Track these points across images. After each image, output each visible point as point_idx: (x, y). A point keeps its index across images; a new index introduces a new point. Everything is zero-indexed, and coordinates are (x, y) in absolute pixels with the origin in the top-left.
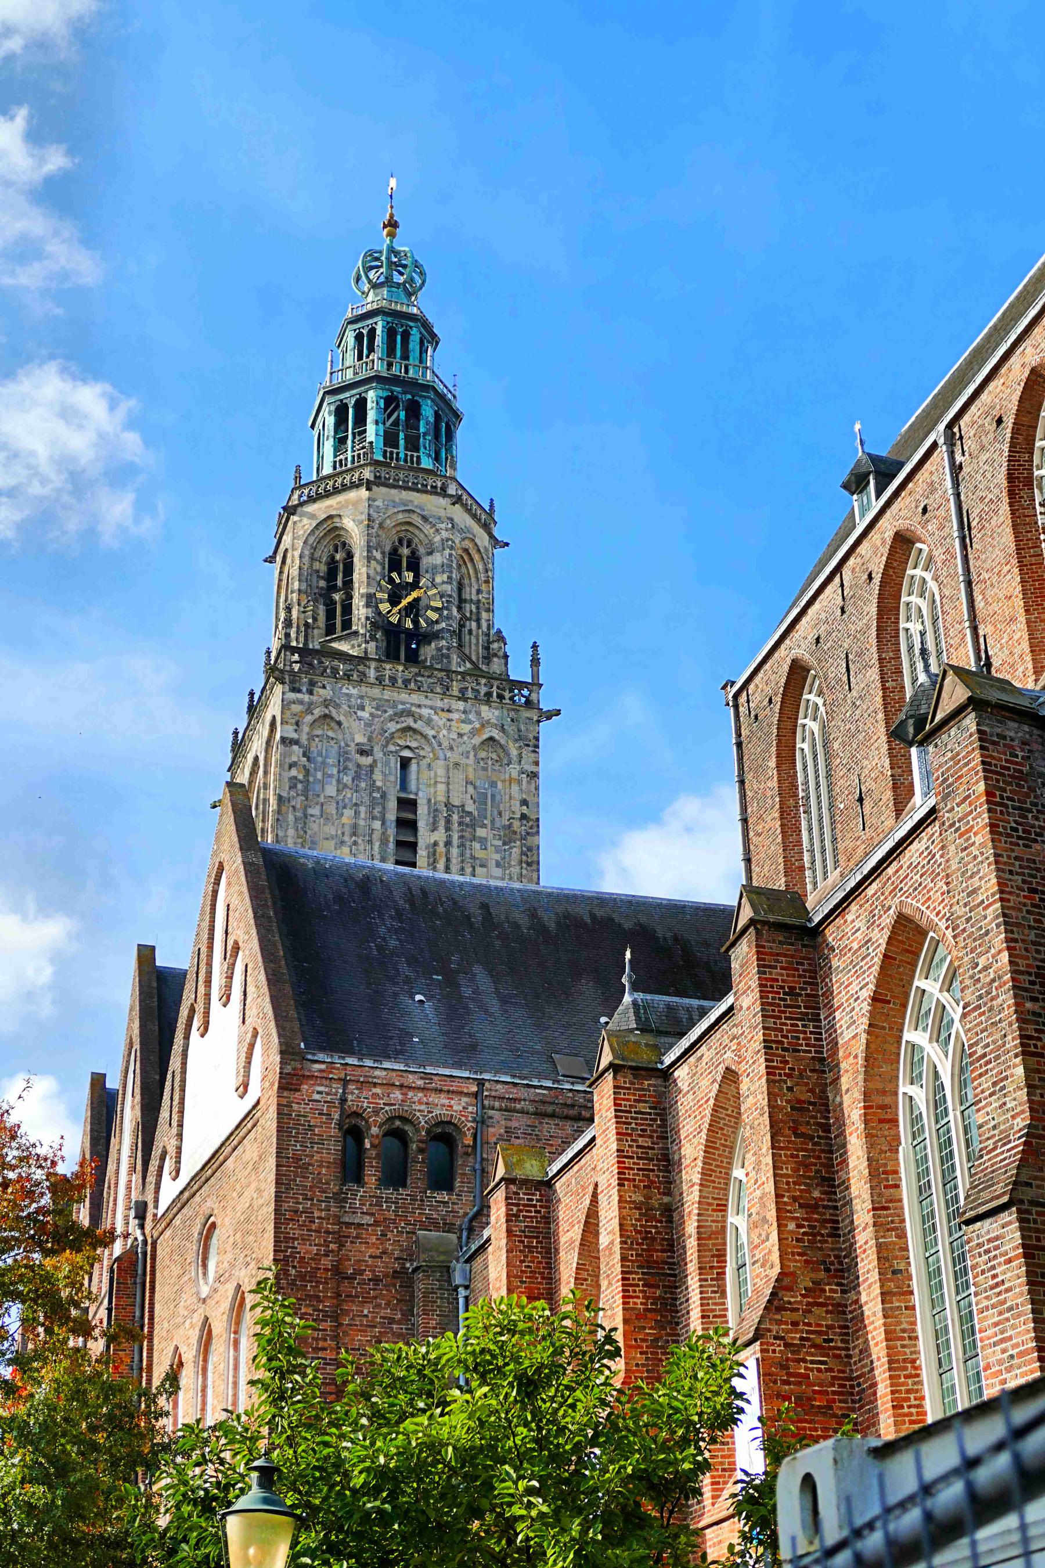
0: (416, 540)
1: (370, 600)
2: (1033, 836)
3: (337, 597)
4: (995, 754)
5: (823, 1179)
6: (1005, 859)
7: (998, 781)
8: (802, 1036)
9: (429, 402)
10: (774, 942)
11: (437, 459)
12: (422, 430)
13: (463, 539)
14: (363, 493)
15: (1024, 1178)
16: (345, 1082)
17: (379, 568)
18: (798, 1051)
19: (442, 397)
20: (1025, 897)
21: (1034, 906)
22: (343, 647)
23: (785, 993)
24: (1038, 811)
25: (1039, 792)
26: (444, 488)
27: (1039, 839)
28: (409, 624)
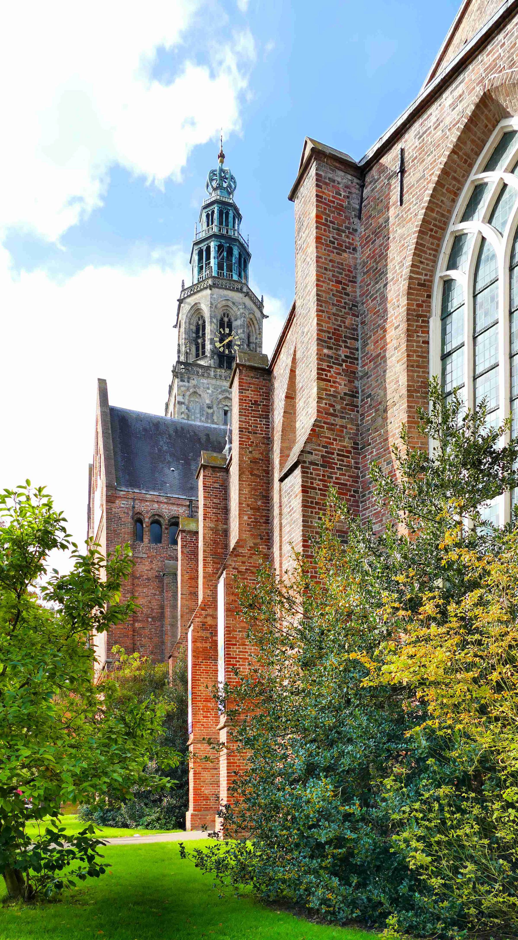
0: (230, 314)
1: (212, 342)
2: (344, 248)
3: (200, 341)
4: (326, 191)
5: (263, 496)
6: (323, 260)
7: (325, 209)
8: (259, 426)
9: (236, 247)
10: (248, 376)
11: (240, 275)
12: (234, 261)
13: (250, 314)
14: (208, 291)
15: (308, 449)
16: (134, 500)
17: (215, 327)
18: (256, 433)
19: (242, 245)
20: (333, 285)
21: (337, 291)
22: (201, 362)
23: (252, 404)
24: (349, 233)
25: (352, 221)
26: (241, 289)
27: (347, 250)
28: (227, 352)
